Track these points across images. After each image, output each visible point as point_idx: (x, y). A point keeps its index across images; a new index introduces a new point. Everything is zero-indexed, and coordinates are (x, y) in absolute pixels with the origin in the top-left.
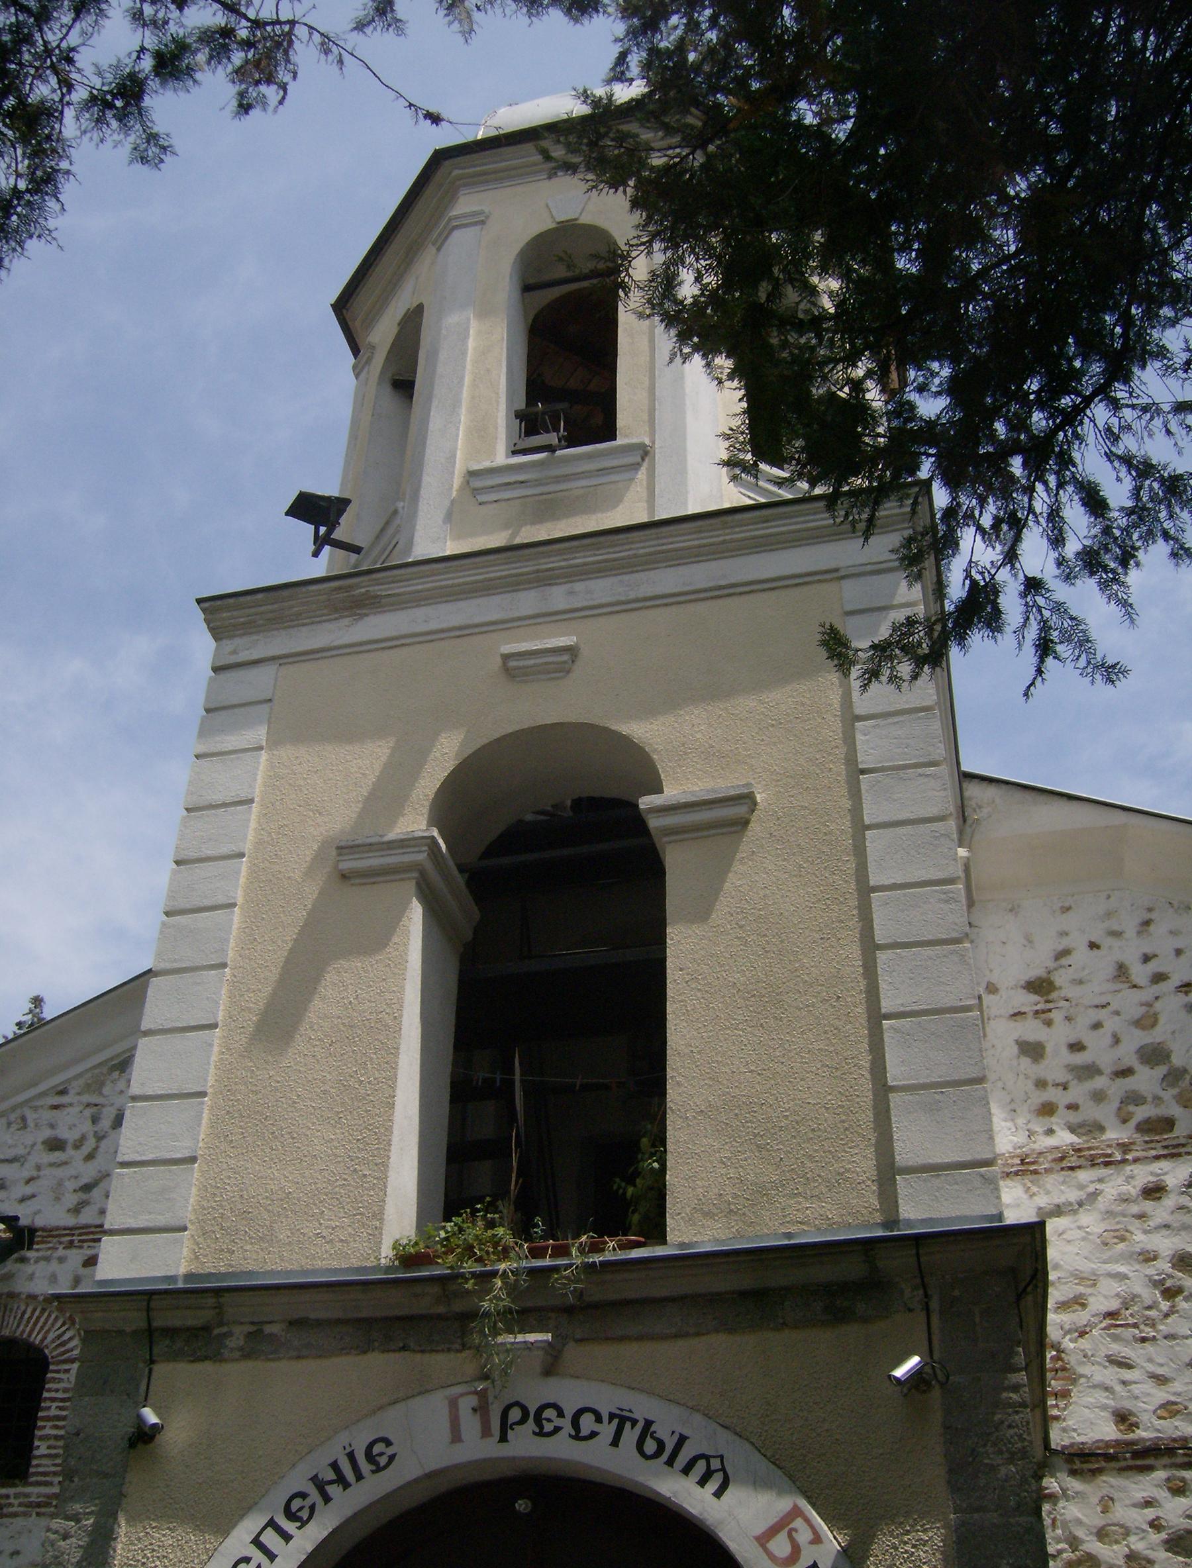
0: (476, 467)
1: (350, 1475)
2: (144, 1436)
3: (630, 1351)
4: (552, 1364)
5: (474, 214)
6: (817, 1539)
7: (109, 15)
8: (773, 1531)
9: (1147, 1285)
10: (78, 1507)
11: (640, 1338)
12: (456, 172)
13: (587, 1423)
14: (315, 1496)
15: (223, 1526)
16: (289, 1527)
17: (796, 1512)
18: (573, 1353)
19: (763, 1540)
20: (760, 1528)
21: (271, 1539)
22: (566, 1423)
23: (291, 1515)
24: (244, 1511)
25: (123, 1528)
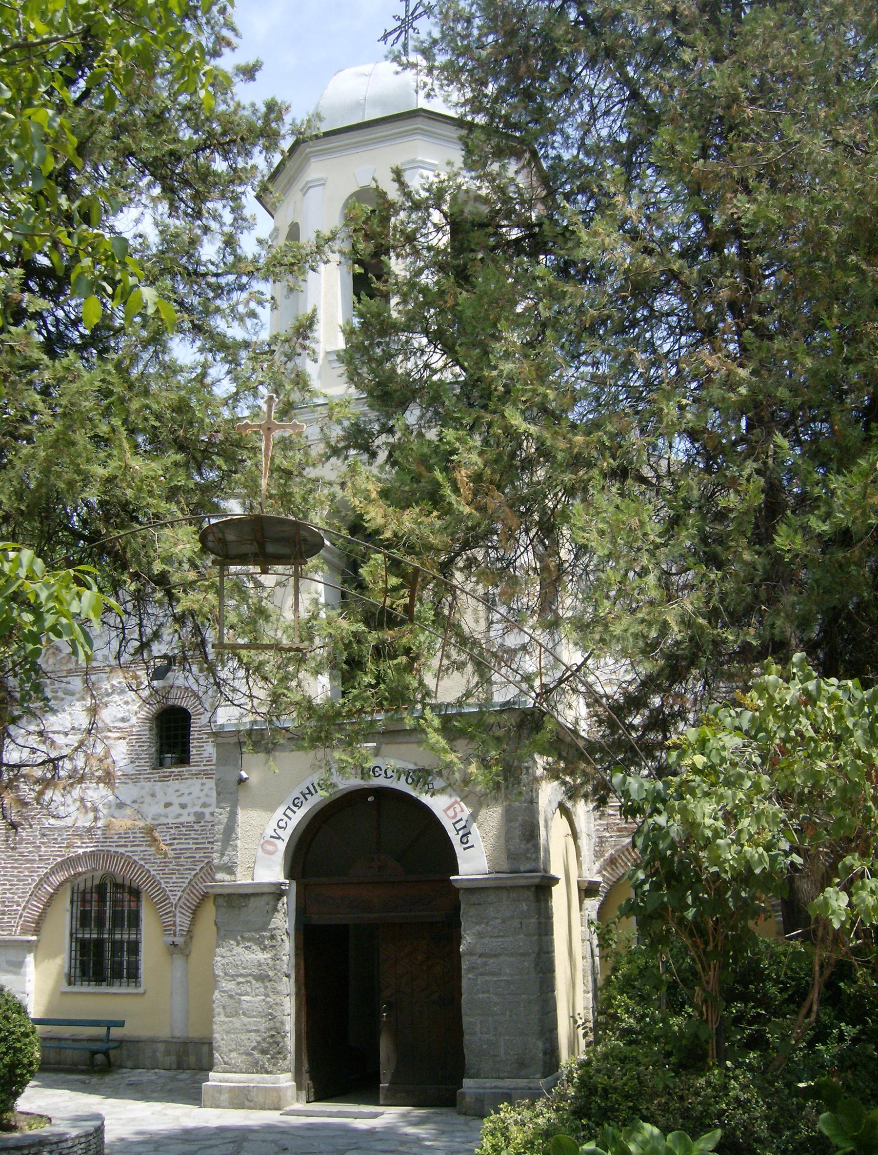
0: (328, 350)
1: (313, 791)
2: (241, 781)
3: (403, 748)
4: (377, 752)
5: (319, 180)
6: (462, 811)
7: (309, 311)
8: (449, 808)
9: (318, 117)
10: (224, 805)
11: (407, 743)
12: (308, 150)
13: (282, 824)
14: (302, 798)
15: (272, 809)
16: (295, 809)
17: (456, 802)
18: (385, 749)
19: (446, 811)
20: (445, 807)
21: (289, 812)
22: (383, 772)
23: (295, 805)
24: (279, 804)
25: (239, 811)
